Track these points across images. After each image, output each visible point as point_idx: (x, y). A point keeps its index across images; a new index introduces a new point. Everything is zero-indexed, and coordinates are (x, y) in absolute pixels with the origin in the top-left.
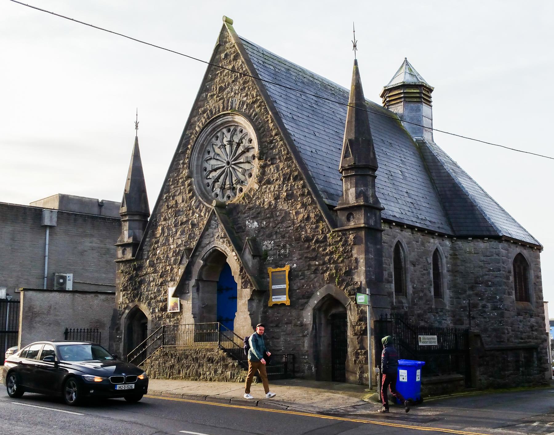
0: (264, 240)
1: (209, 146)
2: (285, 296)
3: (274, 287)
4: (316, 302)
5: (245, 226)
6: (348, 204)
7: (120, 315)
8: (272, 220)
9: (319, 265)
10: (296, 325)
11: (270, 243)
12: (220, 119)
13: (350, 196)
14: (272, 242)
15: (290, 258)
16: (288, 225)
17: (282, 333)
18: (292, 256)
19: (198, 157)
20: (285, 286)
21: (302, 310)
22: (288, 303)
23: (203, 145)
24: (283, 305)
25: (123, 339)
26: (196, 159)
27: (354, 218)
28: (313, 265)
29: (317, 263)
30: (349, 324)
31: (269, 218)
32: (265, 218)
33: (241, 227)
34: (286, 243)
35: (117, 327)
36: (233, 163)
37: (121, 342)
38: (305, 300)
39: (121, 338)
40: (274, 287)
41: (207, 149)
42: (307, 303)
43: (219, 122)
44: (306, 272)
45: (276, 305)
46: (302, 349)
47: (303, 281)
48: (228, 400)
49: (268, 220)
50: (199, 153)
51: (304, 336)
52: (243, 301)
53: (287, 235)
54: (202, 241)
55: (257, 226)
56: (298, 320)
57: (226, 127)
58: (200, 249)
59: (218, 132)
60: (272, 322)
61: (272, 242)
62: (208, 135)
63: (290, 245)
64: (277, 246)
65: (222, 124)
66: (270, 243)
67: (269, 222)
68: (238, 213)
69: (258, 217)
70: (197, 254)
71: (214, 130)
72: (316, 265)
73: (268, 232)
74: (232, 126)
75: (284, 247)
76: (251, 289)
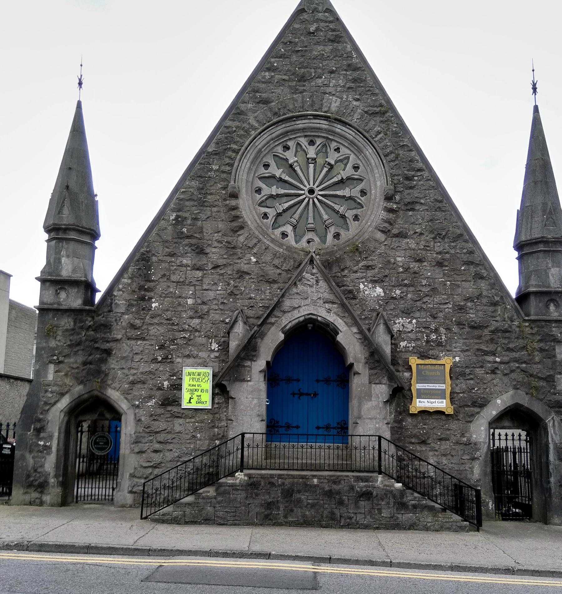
0: (397, 316)
1: (269, 156)
2: (444, 401)
3: (420, 386)
4: (494, 413)
5: (358, 290)
6: (549, 287)
7: (46, 403)
8: (411, 289)
9: (501, 363)
10: (458, 443)
11: (410, 322)
13: (551, 277)
14: (414, 321)
15: (448, 348)
16: (443, 302)
17: (431, 453)
18: (451, 346)
19: (250, 169)
20: (446, 386)
21: (470, 422)
22: (450, 411)
23: (260, 151)
24: (440, 413)
25: (54, 449)
26: (246, 170)
27: (77, 292)
28: (489, 362)
29: (498, 360)
30: (551, 446)
31: (406, 285)
32: (399, 285)
33: (350, 292)
34: (440, 325)
35: (38, 426)
37: (49, 454)
38: (476, 410)
39: (50, 448)
40: (420, 386)
41: (265, 160)
42: (478, 413)
43: (300, 124)
44: (477, 369)
45: (424, 412)
46: (469, 476)
47: (472, 382)
48: (267, 554)
49: (405, 289)
50: (253, 162)
51: (473, 459)
52: (374, 403)
53: (441, 315)
54: (283, 301)
55: (383, 294)
56: (463, 435)
57: (306, 136)
58: (277, 313)
59: (337, 142)
60: (411, 436)
61: (414, 321)
62: (272, 139)
63: (448, 329)
64: (425, 328)
65: (303, 130)
66: (410, 322)
68: (343, 270)
69: (383, 281)
70: (272, 320)
71: (285, 134)
72: (496, 362)
73: (402, 305)
74: (319, 137)
75: (436, 331)
76: (389, 386)
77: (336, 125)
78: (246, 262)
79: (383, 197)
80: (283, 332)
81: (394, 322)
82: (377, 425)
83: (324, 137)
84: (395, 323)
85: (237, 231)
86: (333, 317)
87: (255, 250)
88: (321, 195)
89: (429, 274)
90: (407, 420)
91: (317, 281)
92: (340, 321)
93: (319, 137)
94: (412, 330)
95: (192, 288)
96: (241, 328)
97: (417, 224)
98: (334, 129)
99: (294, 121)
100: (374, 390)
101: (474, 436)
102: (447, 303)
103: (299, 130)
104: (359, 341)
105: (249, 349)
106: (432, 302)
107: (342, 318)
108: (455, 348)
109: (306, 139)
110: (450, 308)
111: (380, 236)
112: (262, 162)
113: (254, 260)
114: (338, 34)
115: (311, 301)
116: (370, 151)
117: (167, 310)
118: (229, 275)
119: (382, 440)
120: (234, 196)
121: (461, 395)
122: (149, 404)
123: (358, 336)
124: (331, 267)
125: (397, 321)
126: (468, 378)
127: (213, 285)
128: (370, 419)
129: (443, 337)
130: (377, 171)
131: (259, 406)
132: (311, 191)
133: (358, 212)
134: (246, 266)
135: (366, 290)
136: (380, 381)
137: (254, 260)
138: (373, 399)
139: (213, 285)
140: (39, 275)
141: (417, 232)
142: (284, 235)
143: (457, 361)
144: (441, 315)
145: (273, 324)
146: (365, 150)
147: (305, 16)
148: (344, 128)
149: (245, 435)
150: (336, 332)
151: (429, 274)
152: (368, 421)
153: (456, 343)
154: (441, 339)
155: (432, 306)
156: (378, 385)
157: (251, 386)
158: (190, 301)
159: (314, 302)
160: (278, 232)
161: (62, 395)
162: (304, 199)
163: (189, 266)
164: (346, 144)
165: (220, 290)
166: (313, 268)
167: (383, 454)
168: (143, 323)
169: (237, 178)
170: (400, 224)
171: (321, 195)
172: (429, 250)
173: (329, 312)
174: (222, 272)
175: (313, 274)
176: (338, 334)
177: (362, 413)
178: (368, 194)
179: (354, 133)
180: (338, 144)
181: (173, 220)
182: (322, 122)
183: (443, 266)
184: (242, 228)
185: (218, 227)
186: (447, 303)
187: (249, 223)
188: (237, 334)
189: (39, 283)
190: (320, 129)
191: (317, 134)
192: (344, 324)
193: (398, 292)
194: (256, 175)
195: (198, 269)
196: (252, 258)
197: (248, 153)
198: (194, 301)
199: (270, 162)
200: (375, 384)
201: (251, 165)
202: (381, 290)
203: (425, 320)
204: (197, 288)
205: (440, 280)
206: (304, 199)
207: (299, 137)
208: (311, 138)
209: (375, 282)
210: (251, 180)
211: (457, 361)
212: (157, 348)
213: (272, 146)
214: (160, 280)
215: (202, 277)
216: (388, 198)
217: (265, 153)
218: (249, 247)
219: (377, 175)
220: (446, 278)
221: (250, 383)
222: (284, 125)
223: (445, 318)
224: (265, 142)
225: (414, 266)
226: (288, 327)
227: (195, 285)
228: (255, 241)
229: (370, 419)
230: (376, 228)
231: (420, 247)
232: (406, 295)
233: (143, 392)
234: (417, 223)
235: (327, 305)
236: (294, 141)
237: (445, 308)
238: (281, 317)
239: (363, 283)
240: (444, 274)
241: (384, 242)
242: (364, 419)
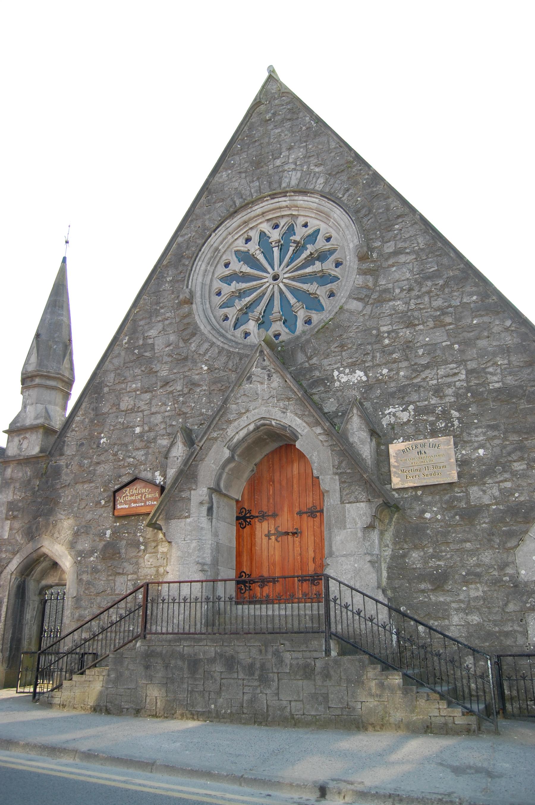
12: (261, 205)
14: (411, 407)
16: (451, 372)
26: (201, 273)
31: (395, 361)
36: (286, 276)
41: (224, 257)
43: (258, 209)
44: (515, 464)
47: (508, 485)
49: (395, 366)
55: (364, 379)
61: (411, 407)
67: (399, 370)
74: (283, 216)
77: (296, 198)
78: (197, 372)
79: (356, 259)
80: (228, 448)
81: (383, 414)
82: (356, 565)
83: (288, 215)
84: (384, 415)
85: (189, 339)
86: (293, 420)
87: (207, 357)
88: (289, 278)
89: (427, 339)
90: (411, 556)
91: (269, 376)
92: (299, 421)
93: (283, 216)
94: (409, 421)
95: (140, 414)
96: (180, 450)
97: (403, 280)
98: (295, 202)
99: (251, 207)
100: (349, 512)
101: (523, 572)
102: (455, 374)
103: (258, 215)
104: (326, 444)
105: (188, 474)
106: (435, 377)
107: (301, 417)
108: (476, 436)
109: (270, 223)
110: (463, 380)
111: (355, 305)
112: (221, 261)
113: (206, 368)
114: (296, 108)
115: (265, 401)
116: (338, 212)
117: (115, 444)
118: (179, 391)
119: (331, 581)
120: (189, 301)
121: (494, 507)
122: (92, 559)
123: (321, 438)
124: (282, 355)
125: (387, 412)
126: (502, 479)
127: (161, 406)
128: (345, 556)
129: (456, 423)
130: (348, 232)
131: (199, 550)
132: (276, 278)
133: (332, 286)
134: (197, 377)
135: (342, 378)
136: (356, 497)
137: (206, 368)
138: (348, 526)
139: (161, 406)
140: (7, 428)
141: (405, 290)
142: (247, 334)
143: (481, 454)
144: (450, 391)
145: (216, 439)
146: (332, 214)
147: (262, 107)
148: (306, 198)
149: (150, 585)
150: (295, 437)
151: (427, 339)
152: (343, 559)
153: (476, 428)
154: (453, 425)
155: (435, 382)
156: (355, 504)
157: (190, 524)
158: (138, 430)
159: (266, 402)
160: (239, 333)
161: (15, 554)
162: (268, 287)
163: (138, 390)
164: (313, 215)
165: (169, 411)
166: (264, 360)
167: (332, 604)
168: (91, 462)
169: (190, 283)
170: (381, 285)
171: (289, 278)
172: (424, 308)
173: (284, 413)
174: (171, 389)
175: (264, 368)
176: (297, 438)
177: (334, 549)
178: (344, 262)
179: (317, 200)
180: (305, 218)
181: (126, 343)
182: (280, 199)
183: (445, 326)
184: (193, 334)
185: (169, 340)
186: (455, 374)
187: (202, 327)
188: (176, 459)
189: (6, 435)
190: (280, 208)
191: (279, 214)
192: (305, 424)
193: (385, 371)
194: (216, 276)
195: (146, 392)
196: (203, 366)
197: (202, 254)
198: (142, 428)
199: (230, 258)
200: (349, 503)
201: (207, 266)
202: (362, 374)
203: (426, 403)
204: (145, 413)
205: (444, 344)
206: (268, 287)
207: (261, 223)
208: (274, 221)
209: (353, 367)
210: (208, 282)
211: (481, 454)
212: (102, 490)
213: (230, 241)
214: (111, 411)
215: (151, 399)
216: (362, 258)
217: (223, 250)
218: (200, 354)
219: (349, 237)
220: (453, 340)
221: (188, 520)
222: (240, 216)
223: (457, 395)
224: (221, 238)
225: (406, 333)
226: (235, 440)
227: (142, 411)
228: (206, 346)
229: (345, 556)
230: (350, 297)
231: (410, 308)
232: (398, 373)
233: (86, 545)
234: (403, 278)
235: (281, 404)
236: (256, 230)
237: (455, 382)
238: (226, 429)
239: (338, 369)
240: (448, 335)
241: (362, 311)
242: (337, 557)
